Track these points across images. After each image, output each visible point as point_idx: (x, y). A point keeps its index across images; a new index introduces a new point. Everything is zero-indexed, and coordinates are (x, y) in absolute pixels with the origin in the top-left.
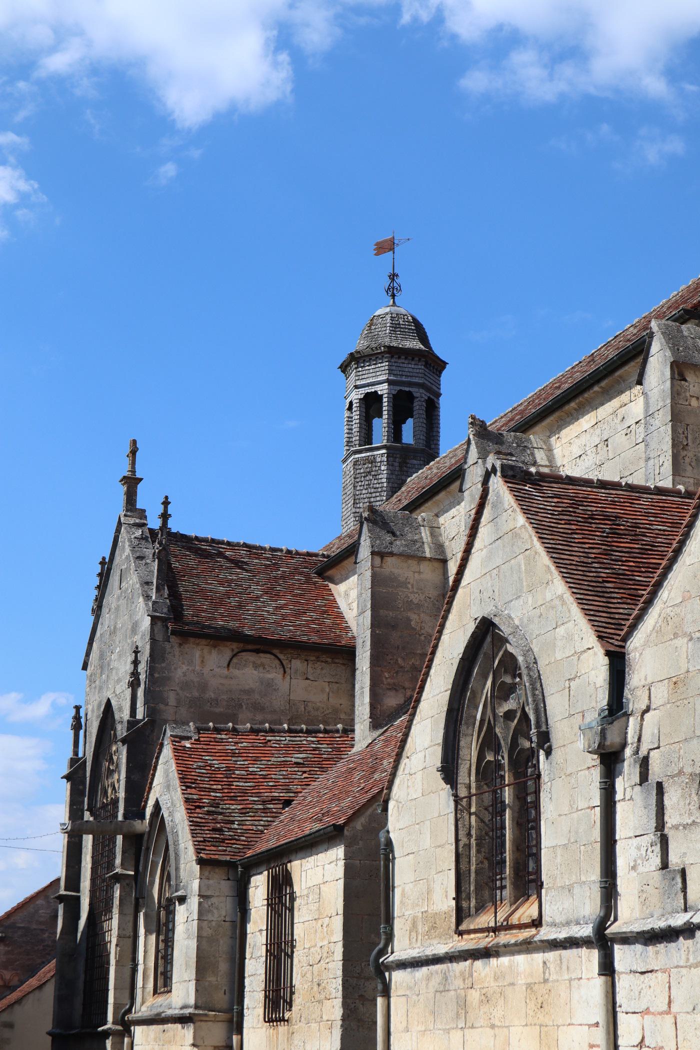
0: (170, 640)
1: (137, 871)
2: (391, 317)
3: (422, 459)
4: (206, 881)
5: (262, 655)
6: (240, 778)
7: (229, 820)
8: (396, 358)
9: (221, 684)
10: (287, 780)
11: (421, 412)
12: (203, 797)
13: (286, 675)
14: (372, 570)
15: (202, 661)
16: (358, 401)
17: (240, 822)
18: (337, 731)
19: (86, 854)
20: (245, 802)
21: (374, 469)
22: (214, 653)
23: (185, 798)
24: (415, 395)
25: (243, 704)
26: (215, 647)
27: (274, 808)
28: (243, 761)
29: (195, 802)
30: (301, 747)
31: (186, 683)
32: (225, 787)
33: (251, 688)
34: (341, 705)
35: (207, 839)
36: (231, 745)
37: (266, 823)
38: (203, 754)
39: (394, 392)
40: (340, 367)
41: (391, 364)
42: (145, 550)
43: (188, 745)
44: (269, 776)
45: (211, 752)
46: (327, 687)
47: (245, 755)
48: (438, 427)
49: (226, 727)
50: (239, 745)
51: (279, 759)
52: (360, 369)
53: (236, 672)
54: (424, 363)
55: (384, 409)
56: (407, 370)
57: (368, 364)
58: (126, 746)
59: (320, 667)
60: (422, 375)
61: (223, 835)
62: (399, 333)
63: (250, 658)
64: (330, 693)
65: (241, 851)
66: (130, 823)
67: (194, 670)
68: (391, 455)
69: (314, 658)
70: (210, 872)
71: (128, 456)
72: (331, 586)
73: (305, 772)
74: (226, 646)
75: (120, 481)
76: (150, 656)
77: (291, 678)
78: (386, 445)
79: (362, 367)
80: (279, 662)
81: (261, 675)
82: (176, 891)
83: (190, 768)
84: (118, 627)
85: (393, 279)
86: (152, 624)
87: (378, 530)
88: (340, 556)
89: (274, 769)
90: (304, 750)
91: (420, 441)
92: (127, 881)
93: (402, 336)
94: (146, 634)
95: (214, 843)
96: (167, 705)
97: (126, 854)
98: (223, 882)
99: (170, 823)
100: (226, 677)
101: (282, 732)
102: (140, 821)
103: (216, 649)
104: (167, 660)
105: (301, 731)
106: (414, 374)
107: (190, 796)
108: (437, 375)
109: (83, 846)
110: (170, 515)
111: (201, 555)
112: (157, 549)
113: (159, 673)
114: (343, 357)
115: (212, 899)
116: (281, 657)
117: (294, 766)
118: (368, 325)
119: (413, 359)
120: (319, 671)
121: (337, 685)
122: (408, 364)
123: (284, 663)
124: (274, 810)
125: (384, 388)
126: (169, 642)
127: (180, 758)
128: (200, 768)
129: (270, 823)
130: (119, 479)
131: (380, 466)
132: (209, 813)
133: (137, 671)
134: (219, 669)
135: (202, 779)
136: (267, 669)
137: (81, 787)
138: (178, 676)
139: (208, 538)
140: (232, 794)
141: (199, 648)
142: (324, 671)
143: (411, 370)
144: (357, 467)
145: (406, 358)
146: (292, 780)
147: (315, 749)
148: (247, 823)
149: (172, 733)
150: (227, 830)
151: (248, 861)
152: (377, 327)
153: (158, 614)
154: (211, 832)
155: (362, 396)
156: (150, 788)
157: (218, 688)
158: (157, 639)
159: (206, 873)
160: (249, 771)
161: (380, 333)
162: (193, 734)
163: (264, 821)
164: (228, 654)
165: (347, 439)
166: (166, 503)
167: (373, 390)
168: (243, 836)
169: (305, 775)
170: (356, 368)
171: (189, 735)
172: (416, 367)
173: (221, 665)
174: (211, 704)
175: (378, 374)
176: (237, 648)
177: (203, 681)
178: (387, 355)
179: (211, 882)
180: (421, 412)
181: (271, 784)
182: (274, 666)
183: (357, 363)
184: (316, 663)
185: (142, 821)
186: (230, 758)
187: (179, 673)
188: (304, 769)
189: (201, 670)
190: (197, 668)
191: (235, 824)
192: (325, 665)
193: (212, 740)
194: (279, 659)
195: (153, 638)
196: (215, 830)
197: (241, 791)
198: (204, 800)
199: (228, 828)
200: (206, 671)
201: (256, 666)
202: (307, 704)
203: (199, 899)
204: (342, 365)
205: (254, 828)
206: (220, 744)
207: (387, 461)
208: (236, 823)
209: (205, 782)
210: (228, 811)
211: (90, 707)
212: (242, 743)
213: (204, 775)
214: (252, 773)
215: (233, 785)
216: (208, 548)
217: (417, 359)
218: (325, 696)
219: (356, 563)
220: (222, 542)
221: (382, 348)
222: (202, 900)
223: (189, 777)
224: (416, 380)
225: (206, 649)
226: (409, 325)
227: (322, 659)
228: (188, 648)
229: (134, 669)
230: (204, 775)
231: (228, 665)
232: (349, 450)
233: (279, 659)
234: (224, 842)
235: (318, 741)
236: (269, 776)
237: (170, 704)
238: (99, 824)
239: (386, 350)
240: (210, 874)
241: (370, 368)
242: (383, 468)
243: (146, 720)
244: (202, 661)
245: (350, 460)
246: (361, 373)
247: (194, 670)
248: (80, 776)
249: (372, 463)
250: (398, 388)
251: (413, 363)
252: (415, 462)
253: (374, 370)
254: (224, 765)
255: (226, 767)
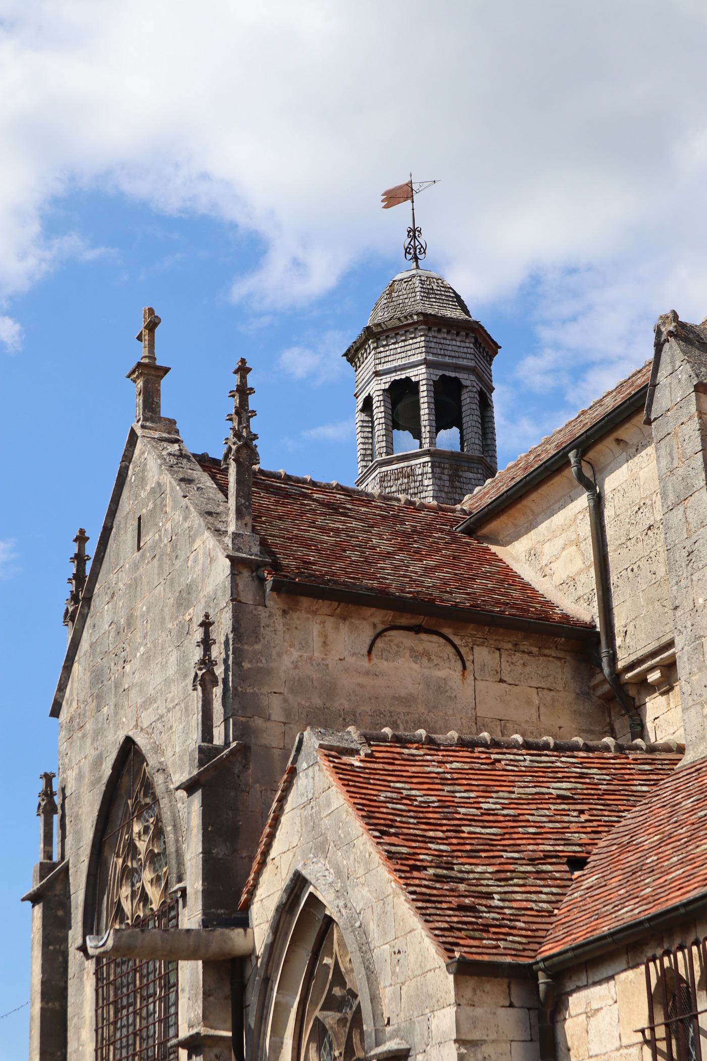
0: (267, 603)
1: (238, 1026)
2: (421, 280)
3: (480, 471)
4: (469, 1009)
5: (423, 636)
6: (472, 820)
7: (481, 892)
8: (435, 331)
9: (358, 684)
10: (558, 825)
11: (474, 406)
12: (418, 851)
13: (467, 672)
14: (700, 418)
15: (325, 642)
16: (381, 393)
17: (503, 896)
18: (607, 748)
19: (78, 1029)
20: (498, 861)
21: (412, 485)
22: (344, 628)
23: (386, 851)
24: (464, 383)
25: (399, 722)
26: (344, 618)
27: (556, 872)
28: (466, 791)
29: (407, 859)
30: (556, 772)
31: (299, 680)
32: (449, 834)
33: (411, 694)
34: (560, 728)
35: (455, 925)
36: (434, 766)
37: (553, 898)
38: (389, 778)
39: (436, 378)
40: (346, 355)
41: (428, 339)
42: (190, 471)
43: (357, 764)
44: (521, 818)
45: (402, 776)
46: (535, 695)
47: (465, 782)
48: (493, 433)
49: (414, 736)
50: (448, 766)
51: (528, 790)
52: (382, 349)
53: (383, 665)
54: (473, 340)
55: (422, 400)
56: (450, 348)
57: (393, 341)
58: (197, 797)
59: (522, 662)
60: (472, 357)
61: (481, 917)
62: (434, 300)
63: (405, 640)
64: (541, 706)
65: (527, 947)
66: (222, 934)
67: (311, 659)
68: (437, 464)
69: (509, 646)
70: (474, 990)
71: (139, 338)
72: (494, 548)
73: (582, 812)
74: (364, 619)
75: (129, 377)
76: (235, 630)
77: (475, 679)
78: (429, 450)
79: (384, 346)
80: (453, 650)
81: (426, 671)
82: (378, 1044)
83: (375, 801)
84: (138, 613)
85: (414, 237)
86: (233, 574)
87: (697, 352)
88: (507, 497)
89: (525, 807)
90: (564, 777)
91: (475, 447)
92: (216, 1051)
93: (438, 304)
94: (219, 593)
95: (472, 933)
96: (268, 719)
97: (212, 999)
98: (502, 1012)
99: (343, 911)
100: (367, 673)
101: (514, 747)
102: (241, 931)
103: (347, 623)
104: (264, 638)
105: (546, 746)
106: (461, 355)
107: (393, 849)
108: (487, 361)
109: (69, 1016)
110: (251, 389)
111: (275, 494)
112: (234, 443)
113: (250, 662)
114: (353, 334)
115: (484, 1048)
116: (457, 641)
117: (558, 801)
118: (387, 292)
119: (458, 334)
120: (519, 668)
121: (552, 693)
122: (452, 340)
123: (463, 651)
124: (558, 875)
125: (420, 372)
126: (265, 606)
127: (351, 783)
128: (392, 800)
129: (558, 898)
130: (128, 373)
131: (422, 480)
132: (438, 878)
133: (210, 658)
134: (354, 658)
135: (404, 819)
136: (435, 662)
137: (60, 913)
138: (283, 668)
139: (280, 473)
140: (468, 848)
141: (319, 619)
142: (528, 669)
143: (456, 348)
144: (385, 484)
145: (448, 332)
146: (565, 825)
147: (582, 776)
148: (518, 897)
149: (321, 742)
150: (484, 909)
151: (576, 956)
152: (400, 293)
153: (244, 555)
154: (457, 913)
155: (387, 386)
156: (263, 864)
157: (354, 692)
158: (243, 600)
159: (468, 994)
160: (481, 808)
161: (407, 301)
162: (359, 746)
163: (546, 894)
164: (367, 635)
165: (363, 452)
166: (243, 370)
167: (403, 377)
168: (519, 921)
169: (583, 818)
170: (375, 348)
171: (352, 746)
172: (463, 344)
173: (357, 651)
174: (344, 719)
175: (409, 353)
176: (383, 622)
177: (328, 678)
178: (423, 327)
179: (479, 1011)
180: (474, 406)
181: (531, 830)
182: (445, 656)
183: (378, 340)
184: (514, 654)
185: (245, 931)
186: (440, 787)
187: (286, 662)
188: (579, 807)
189: (323, 659)
190: (316, 654)
191: (493, 898)
192: (529, 658)
193: (397, 756)
194: (454, 646)
195: (235, 599)
196: (461, 908)
197: (481, 841)
198: (421, 857)
199: (486, 906)
200: (332, 661)
201: (416, 656)
202: (505, 726)
203: (458, 1049)
204: (349, 350)
205: (533, 905)
206: (412, 763)
207: (433, 472)
208: (496, 896)
209: (411, 826)
210: (471, 876)
211: (71, 775)
212: (451, 762)
213: (404, 814)
214: (488, 812)
215: (463, 832)
216: (283, 486)
217: (464, 334)
218: (534, 711)
219: (648, 422)
220: (304, 481)
221: (415, 317)
222: (463, 1050)
223: (377, 815)
224: (465, 362)
225: (330, 622)
226: (447, 292)
227: (522, 648)
228: (299, 619)
229: (204, 656)
230: (404, 814)
231: (370, 652)
232: (365, 466)
233: (454, 646)
234: (488, 932)
235: (581, 763)
236: (521, 818)
237: (273, 718)
238: (166, 935)
239: (421, 318)
240: (475, 994)
241: (397, 346)
242: (426, 482)
243: (233, 745)
244: (325, 642)
245: (372, 476)
246: (383, 355)
247: (311, 659)
248: (57, 892)
249: (408, 477)
250: (441, 373)
251: (458, 339)
252: (471, 475)
253: (403, 349)
254: (434, 798)
255: (439, 801)
